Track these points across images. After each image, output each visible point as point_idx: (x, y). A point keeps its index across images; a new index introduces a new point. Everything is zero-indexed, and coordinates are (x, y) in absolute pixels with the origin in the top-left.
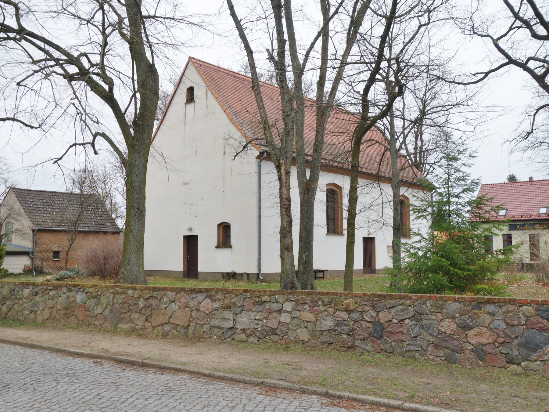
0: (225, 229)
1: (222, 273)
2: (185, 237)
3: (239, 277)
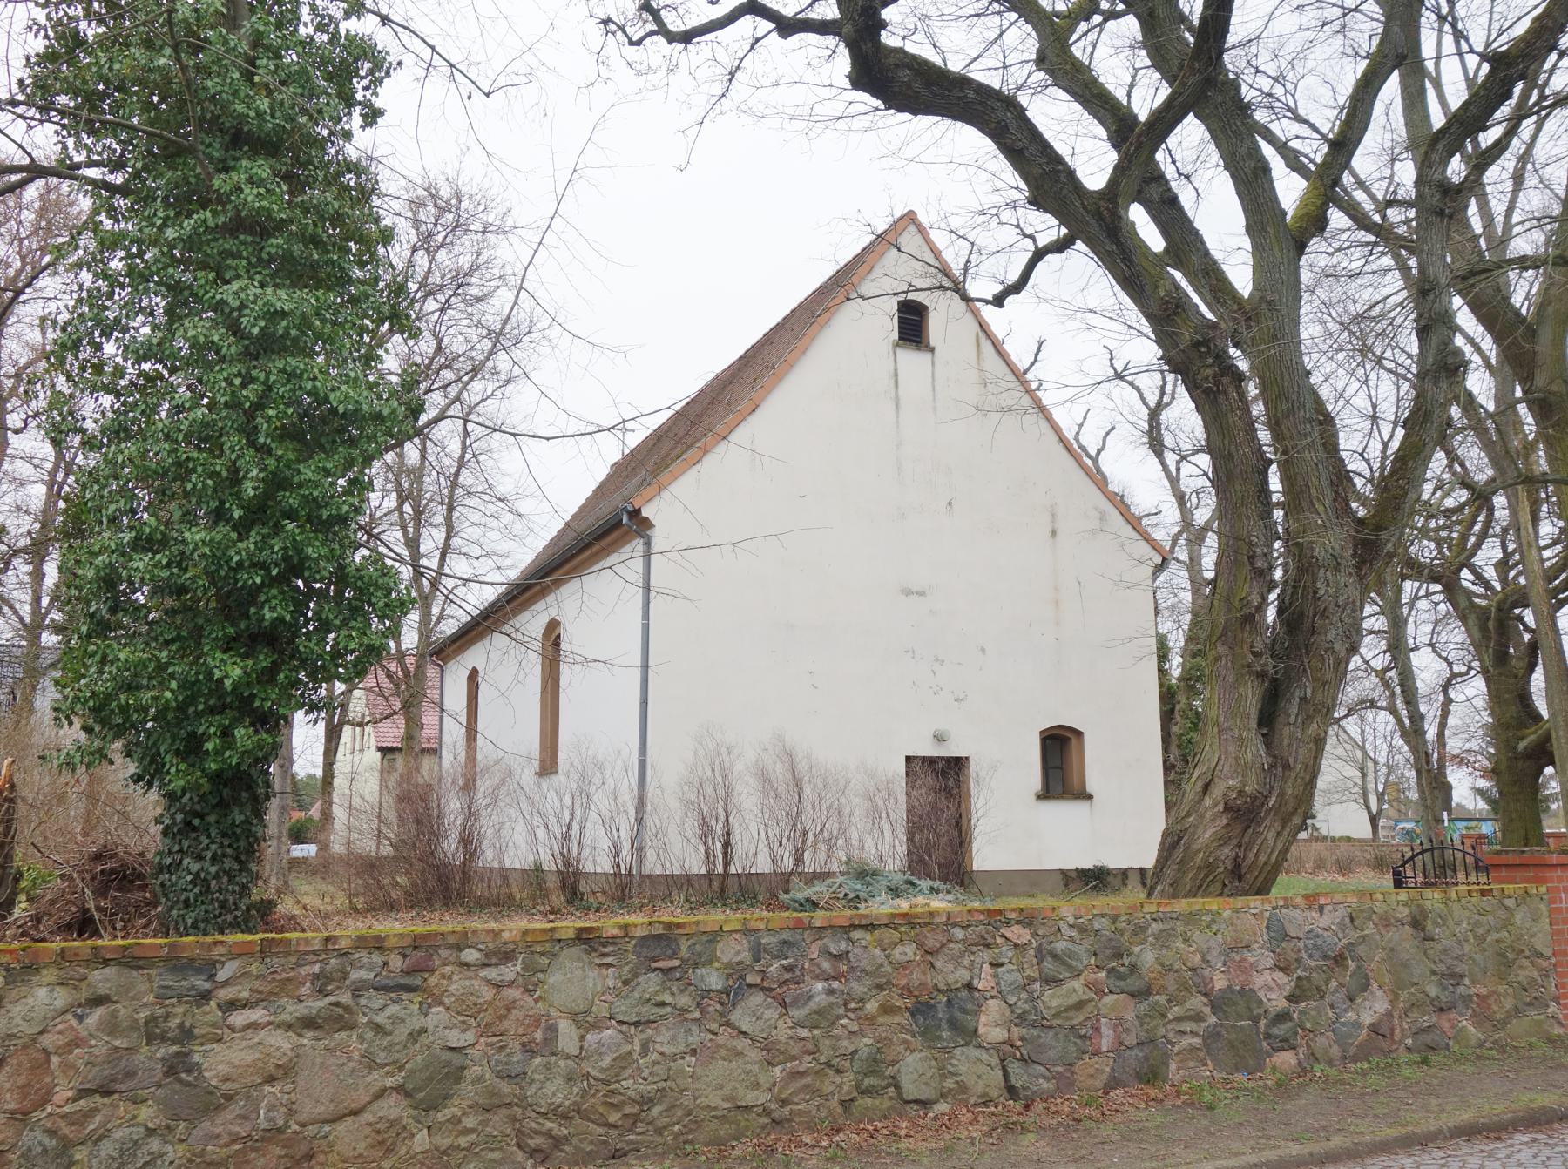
0: (1059, 748)
1: (1062, 872)
3: (1116, 882)
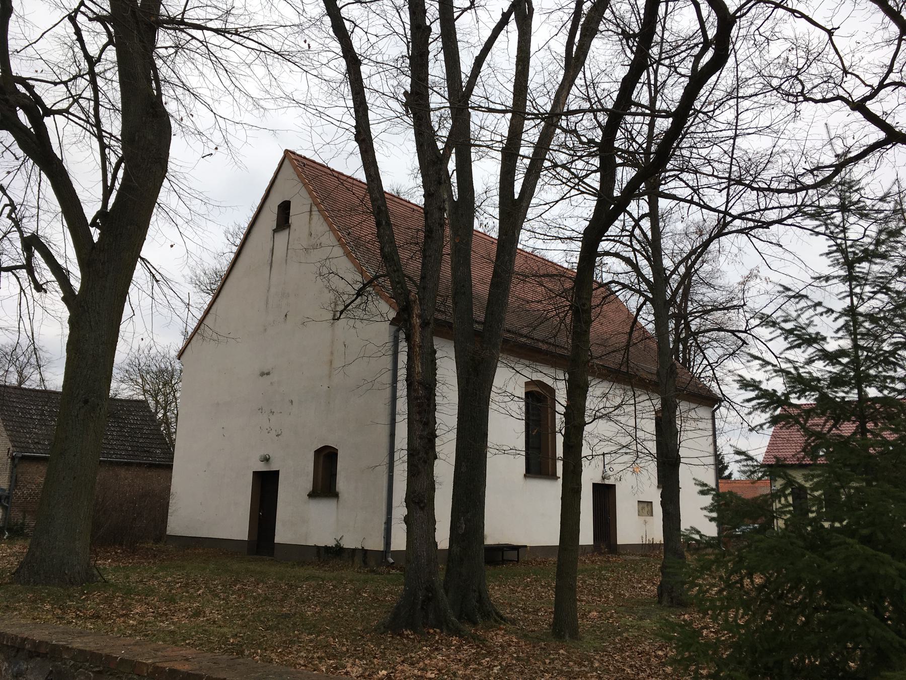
0: (327, 458)
2: (256, 474)
